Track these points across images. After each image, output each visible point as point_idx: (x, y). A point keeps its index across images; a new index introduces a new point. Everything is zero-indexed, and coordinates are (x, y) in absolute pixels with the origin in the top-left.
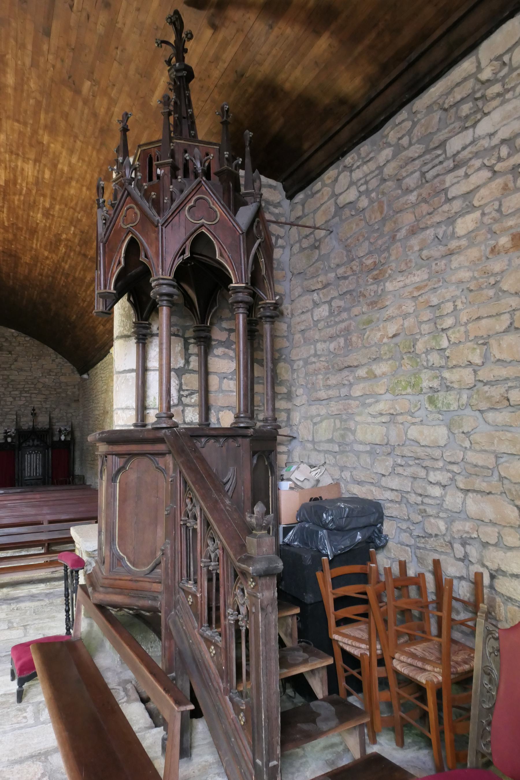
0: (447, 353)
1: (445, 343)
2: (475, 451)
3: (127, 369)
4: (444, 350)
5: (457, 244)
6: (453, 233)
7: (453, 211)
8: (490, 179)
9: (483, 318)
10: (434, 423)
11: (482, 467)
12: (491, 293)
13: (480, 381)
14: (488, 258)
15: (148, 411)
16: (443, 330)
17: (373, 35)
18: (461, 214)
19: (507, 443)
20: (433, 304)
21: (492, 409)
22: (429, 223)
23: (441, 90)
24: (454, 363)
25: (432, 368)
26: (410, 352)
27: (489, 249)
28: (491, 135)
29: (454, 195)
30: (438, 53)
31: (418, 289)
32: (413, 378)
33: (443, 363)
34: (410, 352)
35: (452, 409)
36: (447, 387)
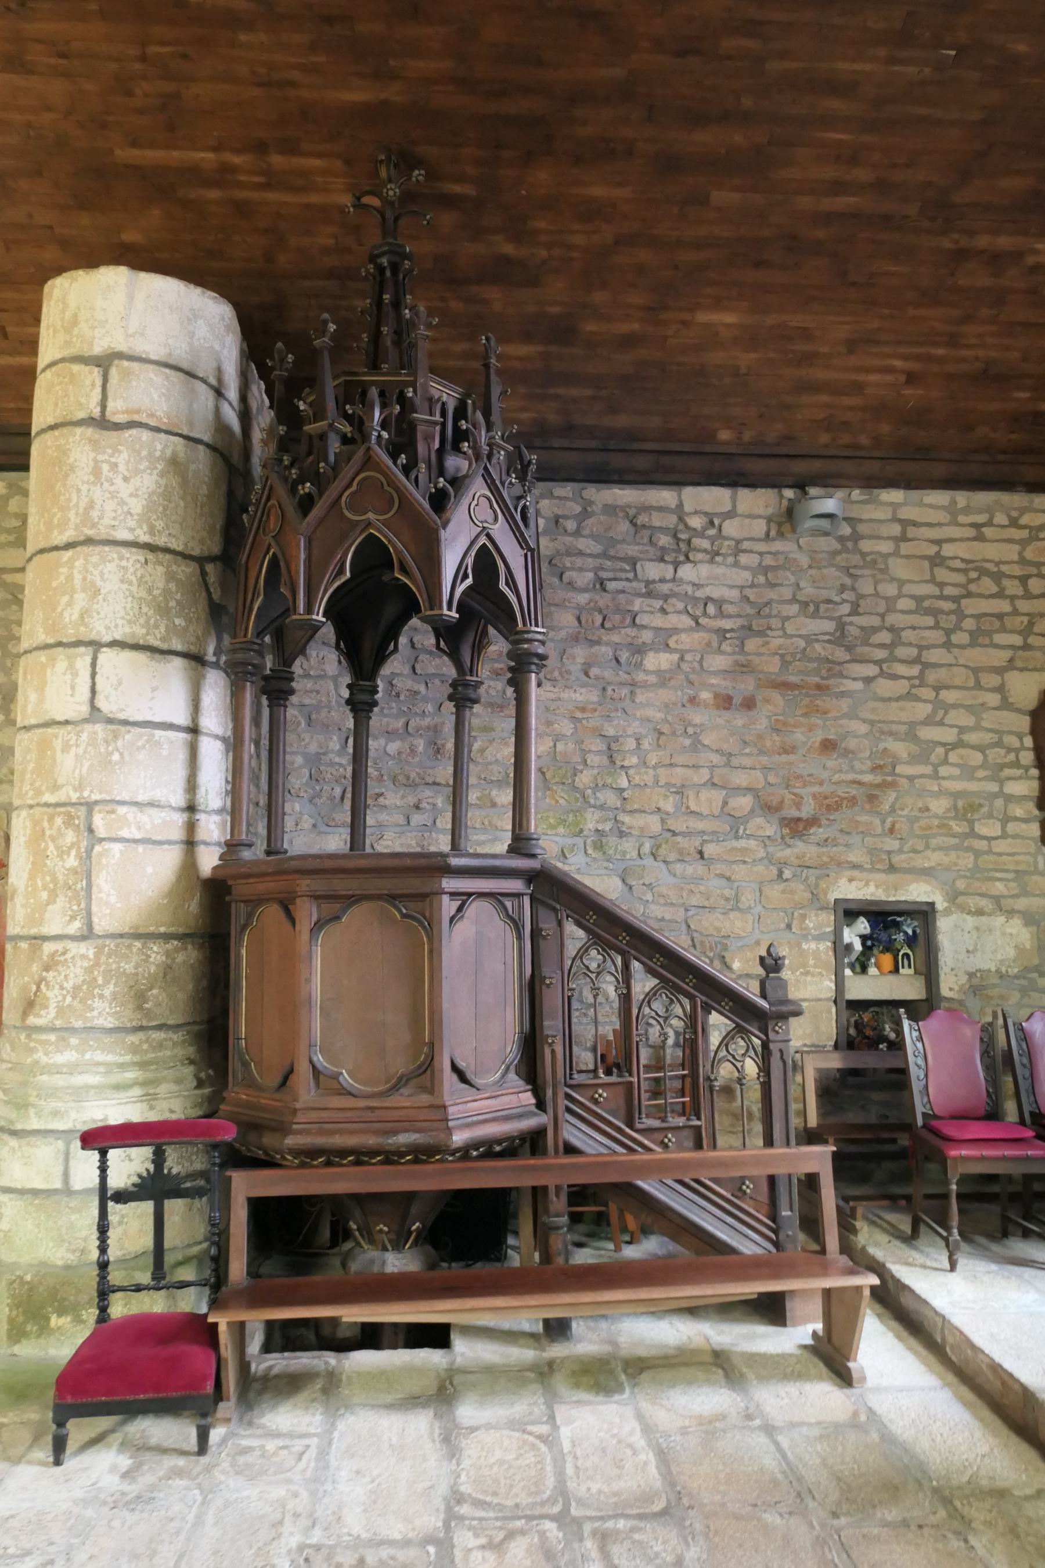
0: (625, 794)
1: (624, 783)
2: (659, 904)
3: (157, 719)
4: (622, 790)
5: (645, 678)
6: (641, 663)
7: (641, 640)
8: (691, 629)
9: (676, 766)
10: (599, 872)
11: (670, 921)
12: (687, 742)
13: (669, 830)
14: (684, 706)
15: (197, 817)
16: (622, 767)
17: (588, 392)
18: (653, 647)
19: (698, 896)
20: (607, 734)
21: (679, 861)
22: (604, 638)
23: (630, 499)
24: (636, 806)
25: (602, 807)
26: (564, 783)
27: (686, 698)
28: (697, 586)
29: (644, 623)
30: (641, 462)
31: (583, 710)
32: (571, 816)
33: (619, 804)
34: (564, 783)
35: (628, 857)
36: (621, 832)
